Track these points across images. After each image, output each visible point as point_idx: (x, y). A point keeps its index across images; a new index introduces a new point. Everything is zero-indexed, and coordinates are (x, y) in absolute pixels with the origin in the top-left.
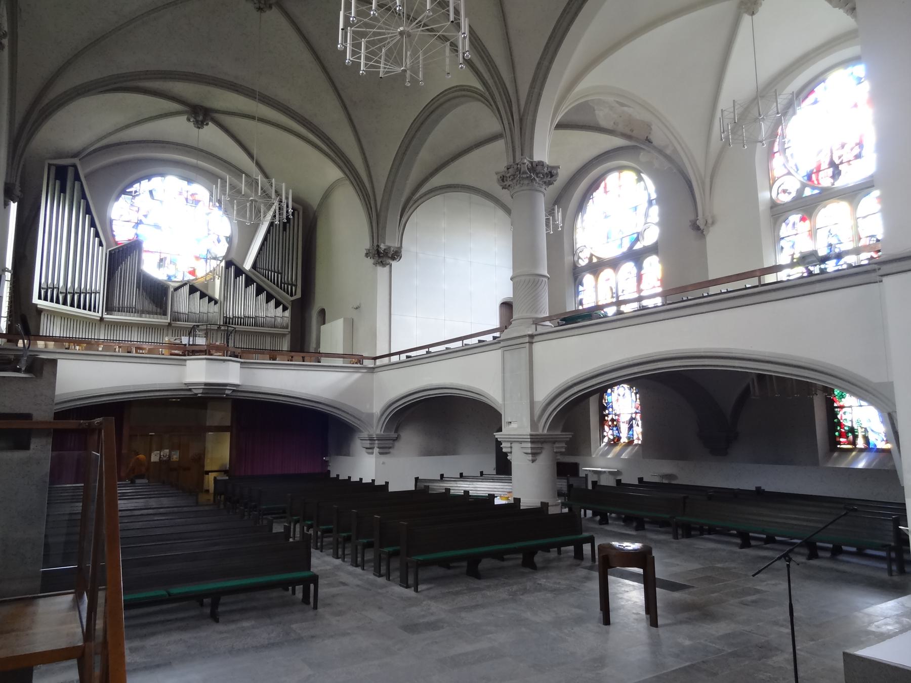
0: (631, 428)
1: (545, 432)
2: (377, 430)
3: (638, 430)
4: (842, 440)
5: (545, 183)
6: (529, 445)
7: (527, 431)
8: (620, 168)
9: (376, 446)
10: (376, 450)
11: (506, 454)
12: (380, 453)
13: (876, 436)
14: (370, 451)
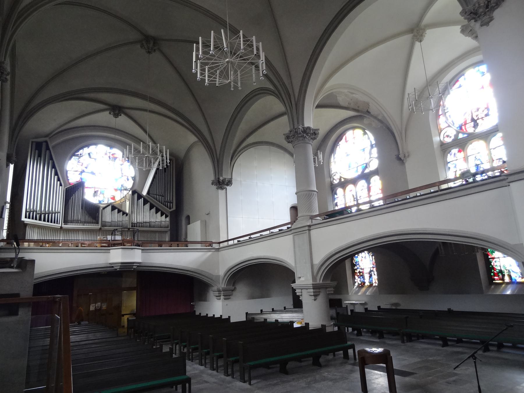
0: (371, 276)
1: (321, 282)
2: (222, 285)
3: (375, 277)
4: (495, 278)
5: (312, 138)
6: (312, 290)
7: (310, 282)
8: (354, 128)
9: (222, 294)
10: (222, 297)
11: (299, 296)
12: (225, 299)
13: (516, 275)
14: (219, 298)
